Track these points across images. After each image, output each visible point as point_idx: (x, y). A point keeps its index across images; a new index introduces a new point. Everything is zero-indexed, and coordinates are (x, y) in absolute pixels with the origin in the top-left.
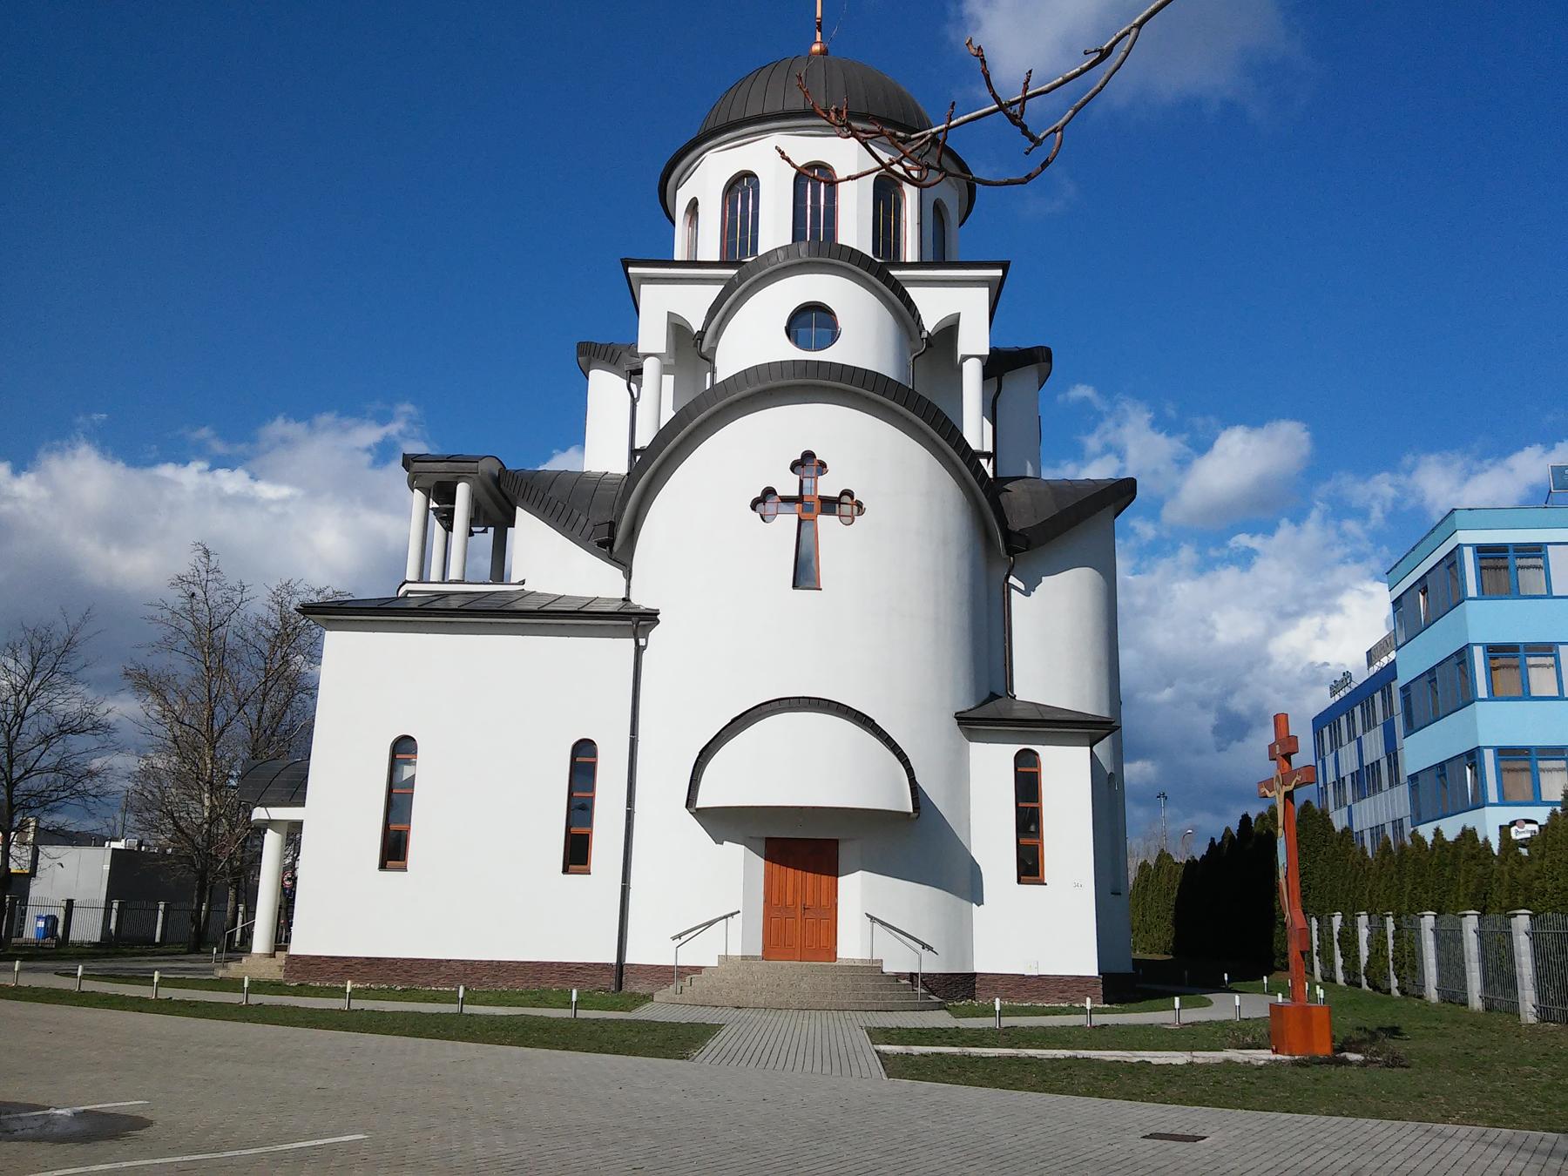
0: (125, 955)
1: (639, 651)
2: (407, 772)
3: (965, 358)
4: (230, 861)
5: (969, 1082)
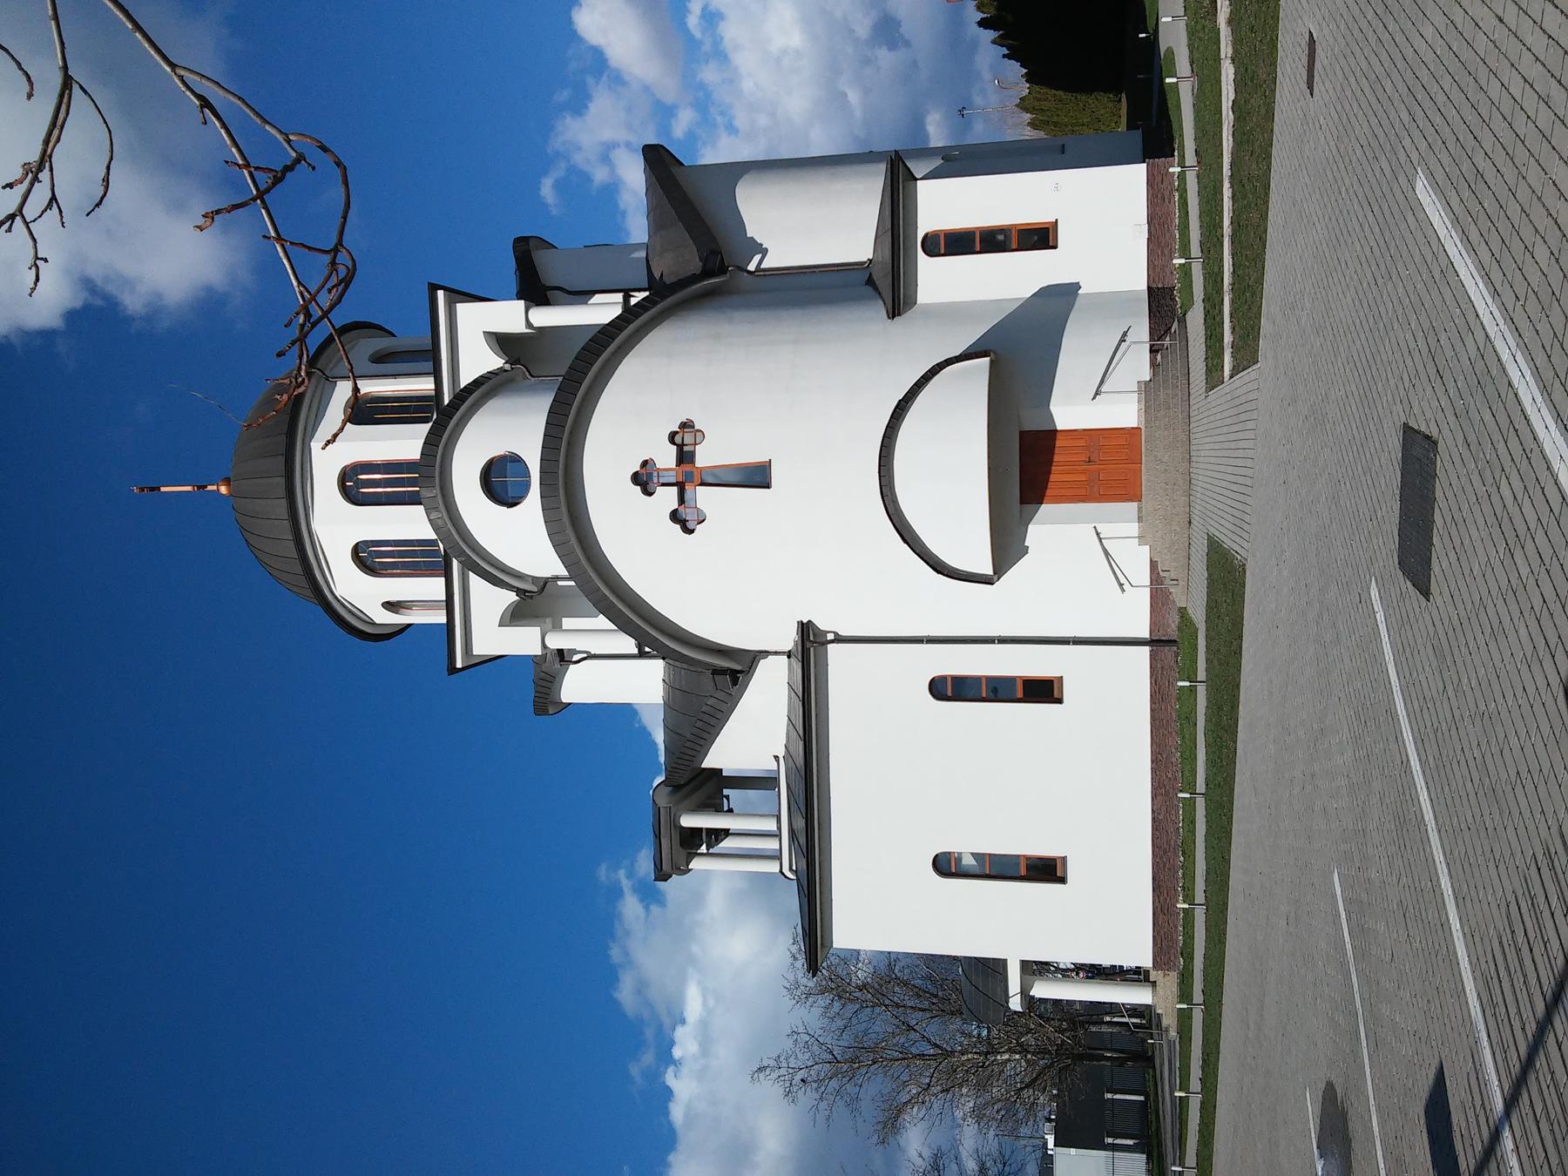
0: (1158, 1128)
1: (839, 639)
2: (968, 861)
3: (529, 324)
4: (1062, 1032)
5: (1260, 281)
